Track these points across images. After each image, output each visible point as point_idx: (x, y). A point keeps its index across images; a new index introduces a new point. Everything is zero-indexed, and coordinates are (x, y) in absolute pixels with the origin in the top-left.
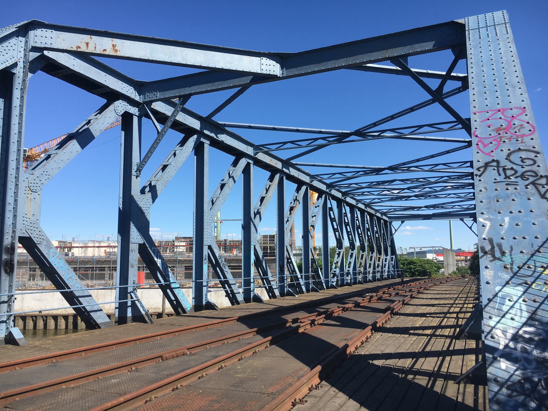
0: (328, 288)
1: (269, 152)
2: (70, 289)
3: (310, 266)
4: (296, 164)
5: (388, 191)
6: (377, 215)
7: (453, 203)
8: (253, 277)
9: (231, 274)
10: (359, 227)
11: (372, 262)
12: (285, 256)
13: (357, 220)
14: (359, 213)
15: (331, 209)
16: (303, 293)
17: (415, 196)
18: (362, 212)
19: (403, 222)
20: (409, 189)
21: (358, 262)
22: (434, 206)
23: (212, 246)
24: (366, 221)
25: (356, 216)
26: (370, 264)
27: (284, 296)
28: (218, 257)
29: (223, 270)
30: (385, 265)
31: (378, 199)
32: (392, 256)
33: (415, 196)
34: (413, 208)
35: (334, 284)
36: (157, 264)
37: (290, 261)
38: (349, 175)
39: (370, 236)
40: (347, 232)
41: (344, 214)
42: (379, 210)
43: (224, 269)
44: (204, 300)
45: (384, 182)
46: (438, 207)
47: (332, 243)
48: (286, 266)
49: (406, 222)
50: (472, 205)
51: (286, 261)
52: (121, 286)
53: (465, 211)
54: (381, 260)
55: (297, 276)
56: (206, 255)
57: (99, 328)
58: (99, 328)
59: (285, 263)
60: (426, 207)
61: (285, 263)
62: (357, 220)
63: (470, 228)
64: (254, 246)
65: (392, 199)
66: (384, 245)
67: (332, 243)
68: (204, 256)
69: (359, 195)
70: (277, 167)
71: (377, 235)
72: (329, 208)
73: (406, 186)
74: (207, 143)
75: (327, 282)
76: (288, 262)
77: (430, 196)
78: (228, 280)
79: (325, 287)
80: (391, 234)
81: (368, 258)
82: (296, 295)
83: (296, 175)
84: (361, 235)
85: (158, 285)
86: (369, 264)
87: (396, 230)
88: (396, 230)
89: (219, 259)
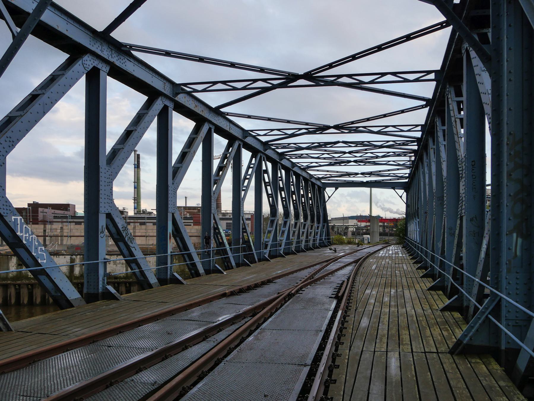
0: (260, 260)
1: (193, 93)
2: (42, 266)
3: (241, 237)
4: (228, 114)
5: (328, 154)
6: (311, 180)
7: (389, 170)
8: (171, 252)
9: (140, 251)
10: (293, 193)
11: (306, 230)
12: (212, 225)
13: (292, 185)
14: (283, 172)
15: (266, 171)
16: (232, 268)
17: (355, 161)
18: (298, 176)
19: (336, 189)
20: (350, 153)
21: (279, 232)
22: (371, 174)
23: (112, 214)
24: (310, 190)
25: (279, 175)
26: (294, 232)
27: (210, 273)
28: (121, 229)
29: (129, 246)
30: (311, 233)
31: (316, 163)
32: (324, 224)
33: (355, 161)
34: (349, 174)
35: (266, 256)
36: (22, 242)
37: (217, 231)
38: (290, 132)
39: (305, 203)
40: (282, 198)
41: (280, 177)
42: (298, 163)
43: (130, 244)
44: (169, 273)
45: (326, 144)
46: (374, 175)
47: (266, 209)
48: (212, 238)
49: (340, 189)
50: (406, 174)
51: (212, 231)
52: (18, 270)
53: (398, 179)
54: (314, 228)
55: (226, 250)
56: (102, 226)
57: (72, 306)
58: (72, 306)
59: (212, 235)
60: (362, 174)
61: (212, 235)
62: (292, 185)
63: (401, 197)
64: (173, 214)
65: (330, 164)
66: (317, 212)
67: (266, 209)
68: (100, 227)
69: (296, 158)
70: (203, 115)
71: (303, 199)
72: (263, 170)
73: (347, 150)
74: (104, 69)
75: (259, 254)
76: (215, 233)
77: (369, 162)
78: (136, 259)
79: (233, 264)
80: (325, 202)
81: (301, 226)
82: (224, 270)
83: (227, 129)
84: (284, 199)
85: (125, 260)
86: (292, 232)
87: (329, 197)
88: (329, 197)
89: (122, 232)
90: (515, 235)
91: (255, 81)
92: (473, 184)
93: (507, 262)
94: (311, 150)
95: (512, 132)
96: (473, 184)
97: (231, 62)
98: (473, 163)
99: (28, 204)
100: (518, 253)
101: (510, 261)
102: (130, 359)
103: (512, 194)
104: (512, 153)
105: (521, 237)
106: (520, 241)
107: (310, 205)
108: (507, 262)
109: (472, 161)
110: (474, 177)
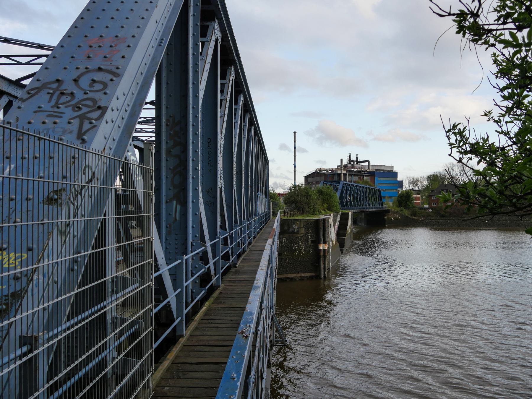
90: (175, 202)
91: (39, 56)
92: (209, 159)
93: (168, 226)
94: (142, 124)
95: (172, 115)
96: (209, 159)
97: (5, 38)
98: (209, 141)
99: (402, 181)
100: (178, 218)
101: (170, 225)
102: (226, 363)
103: (171, 168)
104: (171, 133)
105: (180, 204)
106: (179, 207)
107: (123, 175)
108: (168, 226)
109: (208, 139)
110: (210, 153)
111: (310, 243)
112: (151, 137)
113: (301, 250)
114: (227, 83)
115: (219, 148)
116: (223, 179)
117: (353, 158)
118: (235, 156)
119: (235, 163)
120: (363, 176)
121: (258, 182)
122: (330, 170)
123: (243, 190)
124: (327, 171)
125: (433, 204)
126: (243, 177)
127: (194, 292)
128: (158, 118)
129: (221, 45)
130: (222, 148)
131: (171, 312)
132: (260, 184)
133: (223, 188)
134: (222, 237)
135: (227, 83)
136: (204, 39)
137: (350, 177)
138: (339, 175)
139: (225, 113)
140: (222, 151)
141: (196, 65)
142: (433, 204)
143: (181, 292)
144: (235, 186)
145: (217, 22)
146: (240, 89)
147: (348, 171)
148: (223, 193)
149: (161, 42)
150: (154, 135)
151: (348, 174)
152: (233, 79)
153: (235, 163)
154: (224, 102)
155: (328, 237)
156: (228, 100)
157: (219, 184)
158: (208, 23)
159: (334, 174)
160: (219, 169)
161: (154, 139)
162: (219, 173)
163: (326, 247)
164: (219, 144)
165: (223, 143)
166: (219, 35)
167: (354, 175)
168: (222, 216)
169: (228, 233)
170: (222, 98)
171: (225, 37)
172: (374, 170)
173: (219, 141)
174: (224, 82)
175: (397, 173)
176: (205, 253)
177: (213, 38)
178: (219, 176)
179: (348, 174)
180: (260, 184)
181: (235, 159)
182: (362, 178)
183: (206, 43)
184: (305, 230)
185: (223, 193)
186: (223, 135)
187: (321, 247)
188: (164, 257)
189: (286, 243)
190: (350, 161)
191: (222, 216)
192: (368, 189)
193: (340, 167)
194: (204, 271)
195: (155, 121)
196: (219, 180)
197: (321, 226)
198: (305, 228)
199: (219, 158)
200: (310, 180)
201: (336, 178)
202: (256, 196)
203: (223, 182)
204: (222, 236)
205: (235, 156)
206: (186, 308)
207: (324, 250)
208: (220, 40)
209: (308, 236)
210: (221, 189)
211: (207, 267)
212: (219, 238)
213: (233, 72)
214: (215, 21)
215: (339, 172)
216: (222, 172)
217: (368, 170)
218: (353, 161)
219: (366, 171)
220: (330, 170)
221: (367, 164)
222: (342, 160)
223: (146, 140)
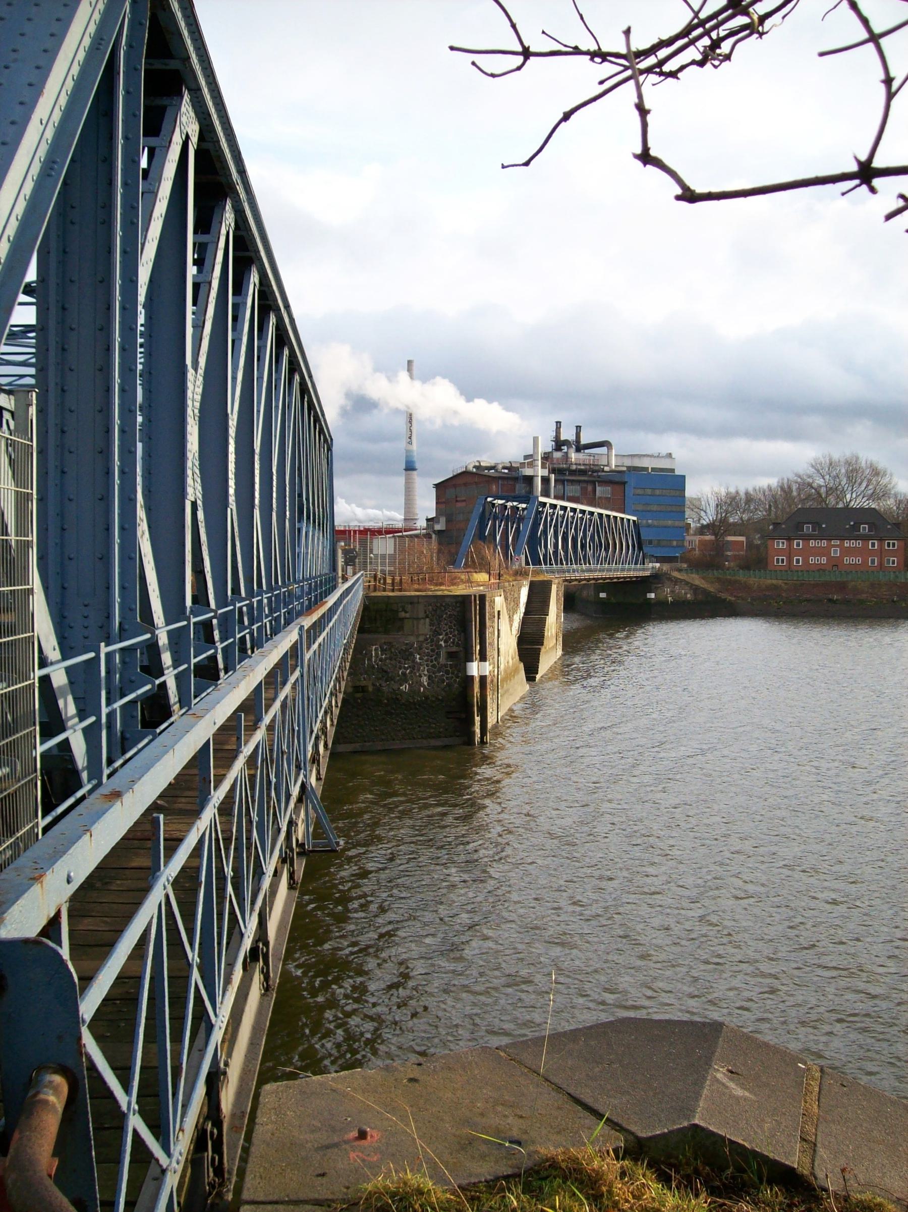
111: (442, 660)
112: (22, 376)
113: (420, 676)
114: (213, 242)
115: (189, 402)
116: (199, 480)
117: (568, 434)
118: (233, 423)
119: (232, 442)
120: (594, 483)
121: (300, 495)
122: (504, 468)
123: (257, 513)
124: (496, 471)
125: (778, 560)
126: (275, 483)
127: (127, 739)
128: (40, 328)
129: (197, 153)
130: (197, 405)
131: (72, 759)
132: (308, 499)
133: (199, 503)
134: (193, 620)
135: (213, 242)
136: (153, 141)
137: (560, 487)
138: (530, 480)
139: (207, 317)
140: (196, 411)
141: (130, 208)
142: (778, 560)
143: (97, 723)
144: (232, 499)
145: (186, 98)
146: (247, 254)
147: (553, 471)
148: (201, 515)
149: (52, 169)
150: (32, 371)
151: (553, 477)
152: (228, 233)
153: (232, 442)
154: (203, 289)
155: (491, 644)
156: (215, 284)
157: (190, 490)
158: (165, 101)
159: (516, 479)
160: (190, 455)
161: (32, 381)
162: (189, 464)
163: (487, 668)
164: (189, 394)
165: (199, 390)
166: (193, 129)
167: (568, 481)
168: (199, 571)
169: (212, 611)
170: (198, 281)
171: (206, 131)
172: (625, 469)
173: (190, 385)
174: (204, 238)
175: (683, 477)
176: (152, 648)
177: (177, 140)
178: (189, 472)
179: (553, 477)
180: (308, 499)
181: (232, 432)
182: (590, 488)
183: (157, 151)
184: (431, 624)
185: (201, 515)
186: (201, 371)
187: (474, 669)
188: (56, 644)
189: (381, 660)
190: (559, 444)
191: (199, 571)
192: (605, 519)
193: (529, 459)
194: (150, 690)
195: (33, 335)
196: (190, 481)
197: (475, 610)
198: (431, 620)
199: (189, 428)
200: (450, 493)
201: (520, 489)
202: (296, 533)
203: (200, 488)
204: (195, 616)
205: (233, 423)
206: (135, 1132)
207: (483, 679)
208: (194, 139)
209: (439, 640)
210: (194, 505)
211: (157, 682)
212: (188, 620)
213: (227, 215)
214: (182, 97)
215: (528, 472)
216: (197, 463)
217: (606, 469)
218: (566, 443)
219: (603, 471)
220: (504, 468)
221: (603, 450)
222: (535, 440)
223: (10, 384)
